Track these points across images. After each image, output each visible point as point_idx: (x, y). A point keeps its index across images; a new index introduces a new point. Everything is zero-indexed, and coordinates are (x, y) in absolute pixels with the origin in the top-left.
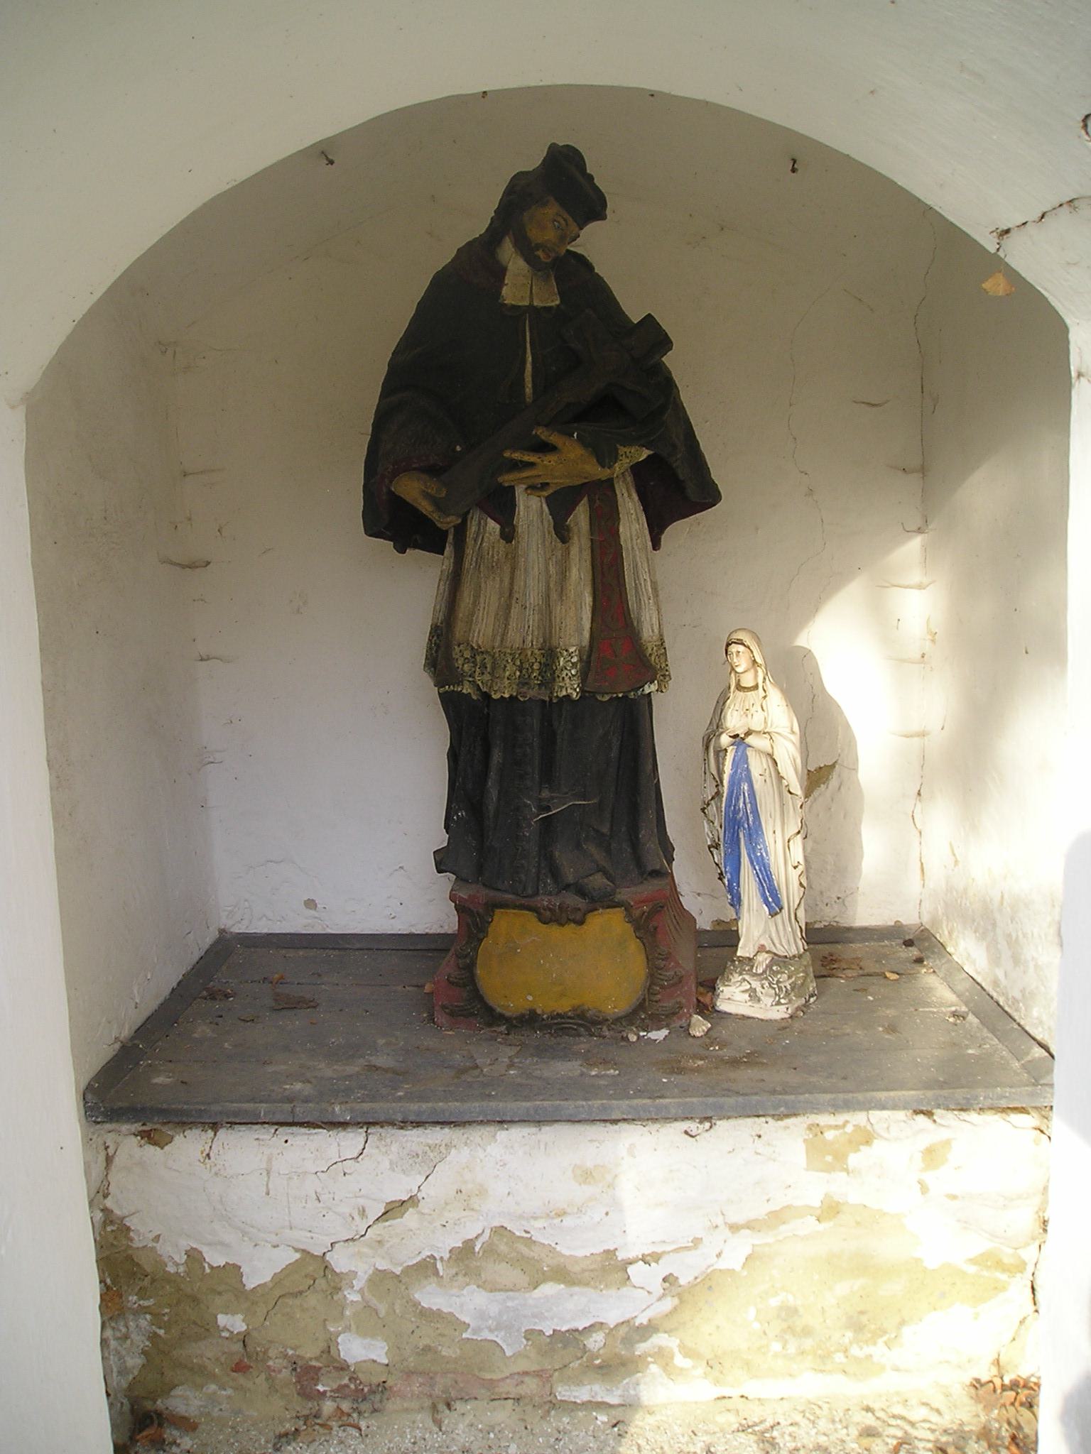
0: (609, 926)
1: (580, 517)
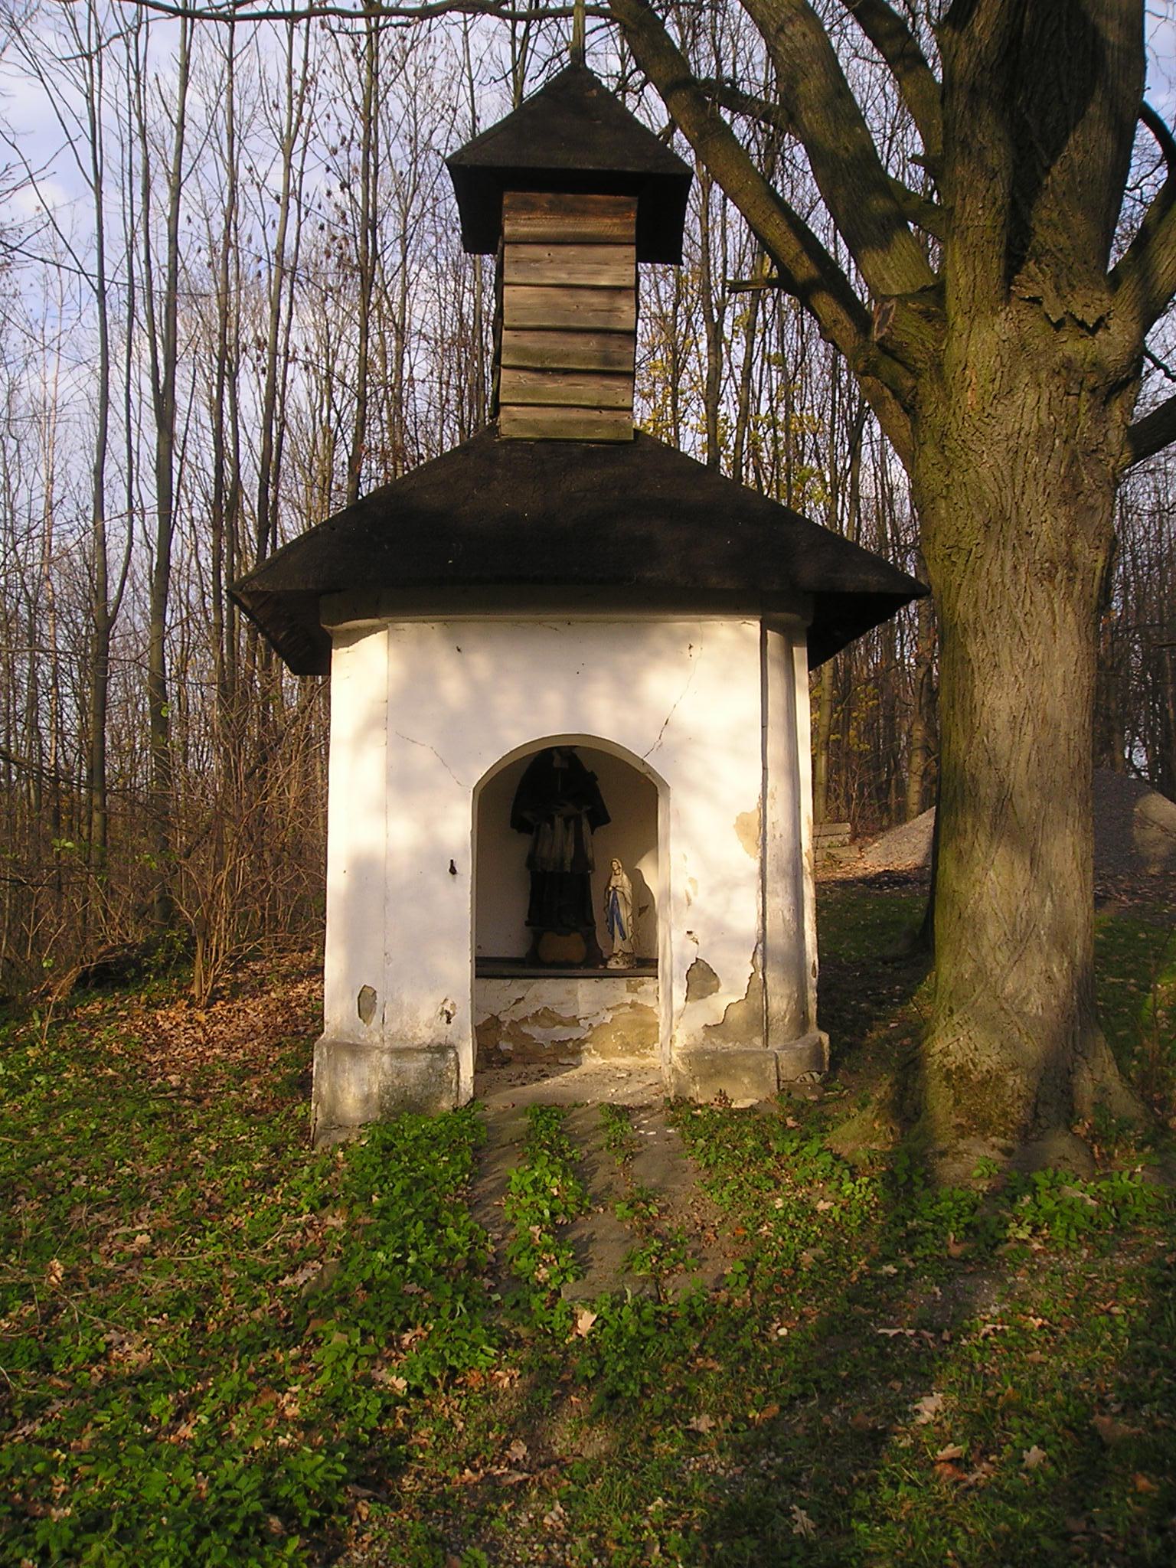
0: (576, 936)
1: (572, 824)
